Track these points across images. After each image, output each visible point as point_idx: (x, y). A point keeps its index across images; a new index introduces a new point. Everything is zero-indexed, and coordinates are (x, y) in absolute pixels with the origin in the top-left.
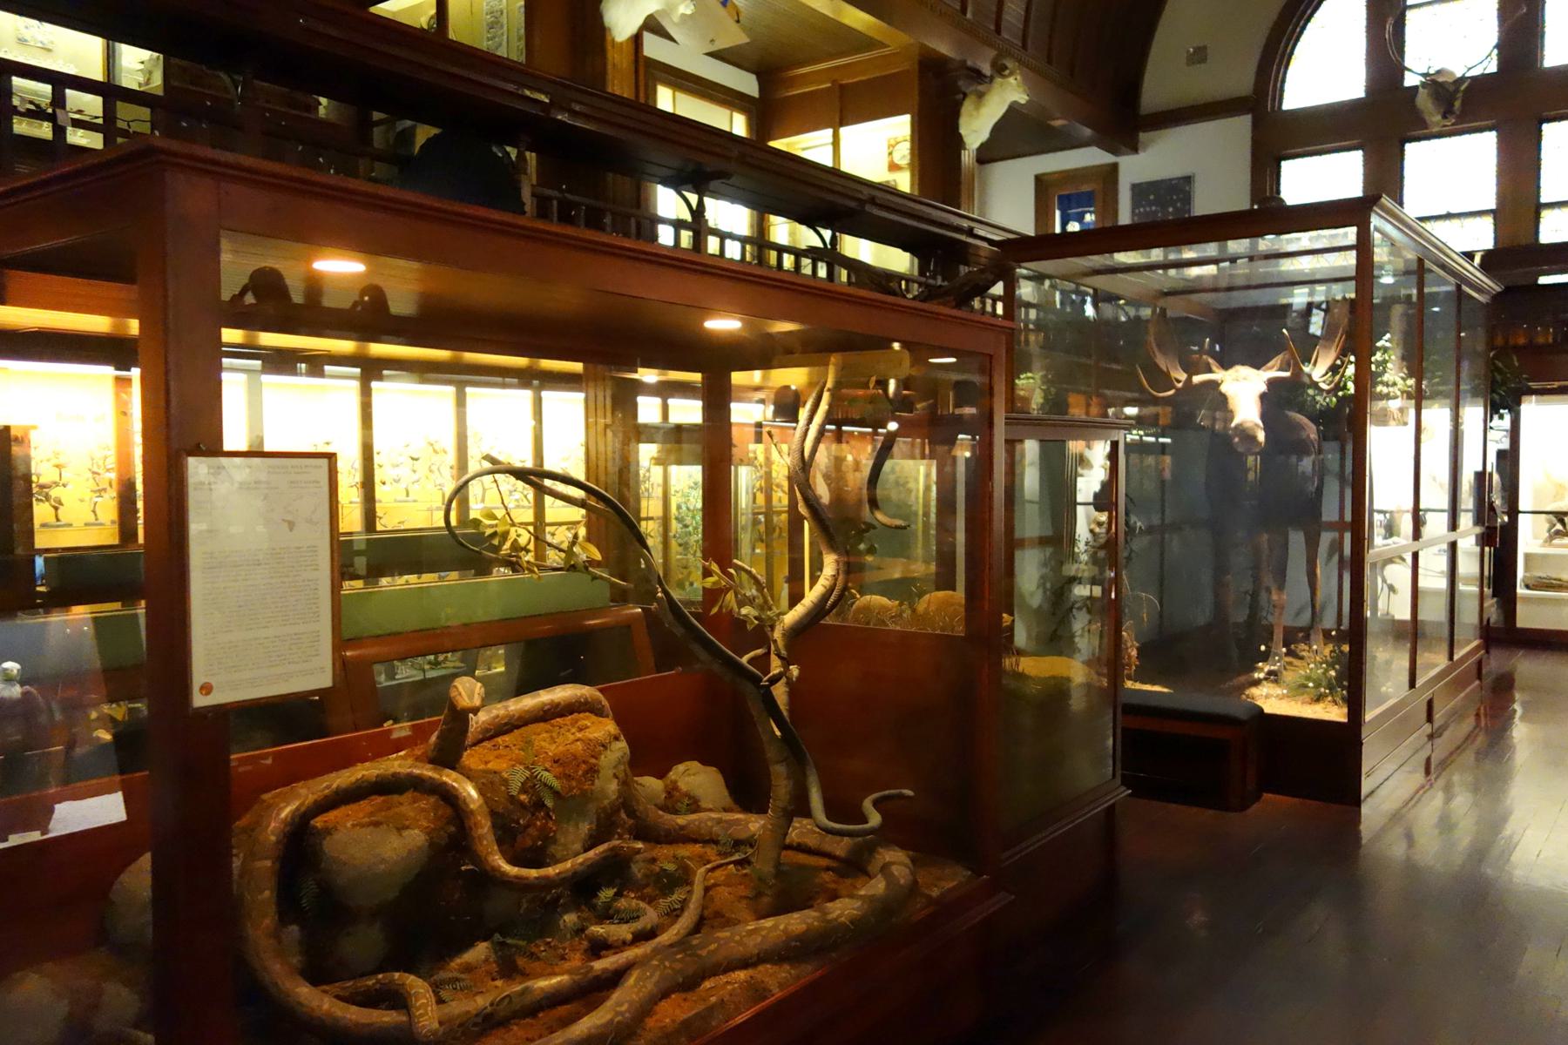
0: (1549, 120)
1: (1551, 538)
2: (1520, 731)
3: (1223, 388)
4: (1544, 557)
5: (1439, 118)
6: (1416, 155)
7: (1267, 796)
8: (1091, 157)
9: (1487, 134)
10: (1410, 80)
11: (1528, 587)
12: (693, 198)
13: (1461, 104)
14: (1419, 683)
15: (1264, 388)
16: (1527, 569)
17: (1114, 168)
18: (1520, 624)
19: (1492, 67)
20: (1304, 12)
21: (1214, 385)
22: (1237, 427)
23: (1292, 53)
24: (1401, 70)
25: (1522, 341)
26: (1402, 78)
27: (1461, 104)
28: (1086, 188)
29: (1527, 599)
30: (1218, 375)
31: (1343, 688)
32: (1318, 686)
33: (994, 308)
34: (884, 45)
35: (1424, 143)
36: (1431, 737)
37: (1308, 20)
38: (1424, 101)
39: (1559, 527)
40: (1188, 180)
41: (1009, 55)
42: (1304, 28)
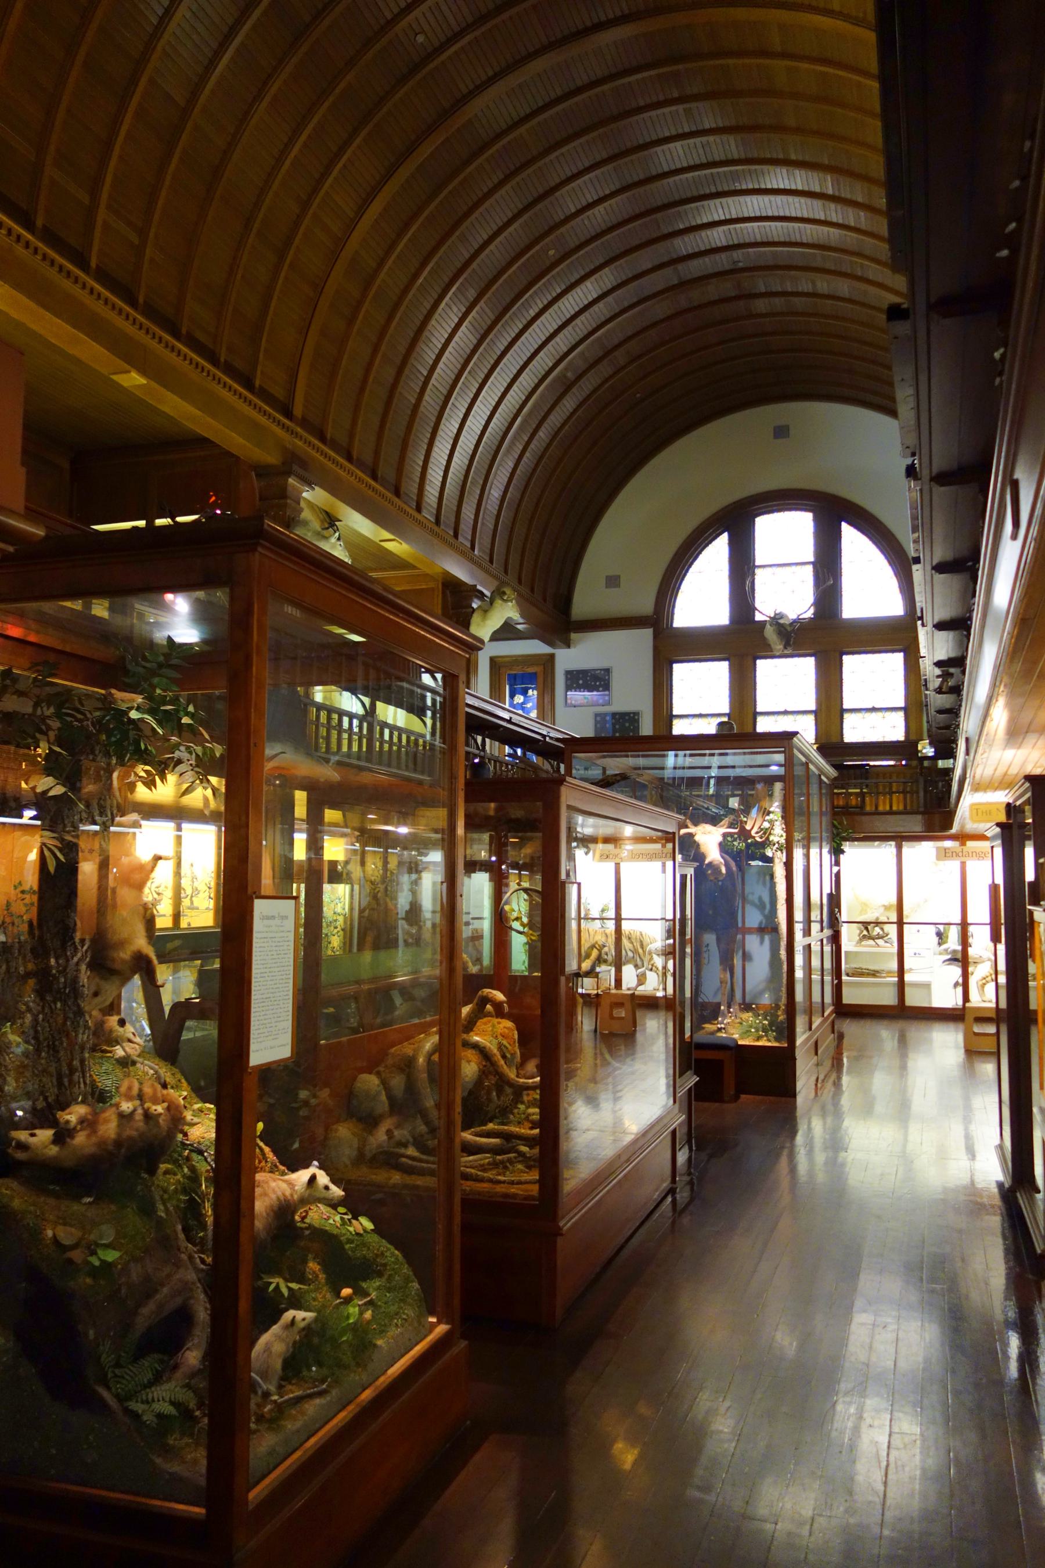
0: (848, 653)
1: (861, 940)
2: (845, 1079)
3: (697, 838)
4: (856, 953)
5: (781, 647)
6: (765, 668)
7: (743, 1096)
8: (535, 647)
9: (808, 658)
10: (758, 617)
11: (848, 975)
12: (367, 701)
13: (795, 638)
14: (814, 1027)
15: (721, 839)
16: (846, 963)
17: (552, 657)
18: (845, 1001)
19: (810, 614)
20: (687, 561)
21: (691, 836)
22: (710, 863)
23: (679, 588)
24: (752, 609)
25: (841, 803)
26: (754, 616)
27: (795, 638)
28: (530, 670)
29: (850, 983)
30: (692, 829)
31: (773, 1031)
32: (757, 1031)
33: (318, 717)
34: (414, 567)
35: (769, 661)
36: (817, 1065)
37: (690, 566)
38: (770, 632)
39: (865, 933)
40: (607, 671)
41: (508, 584)
42: (687, 571)
